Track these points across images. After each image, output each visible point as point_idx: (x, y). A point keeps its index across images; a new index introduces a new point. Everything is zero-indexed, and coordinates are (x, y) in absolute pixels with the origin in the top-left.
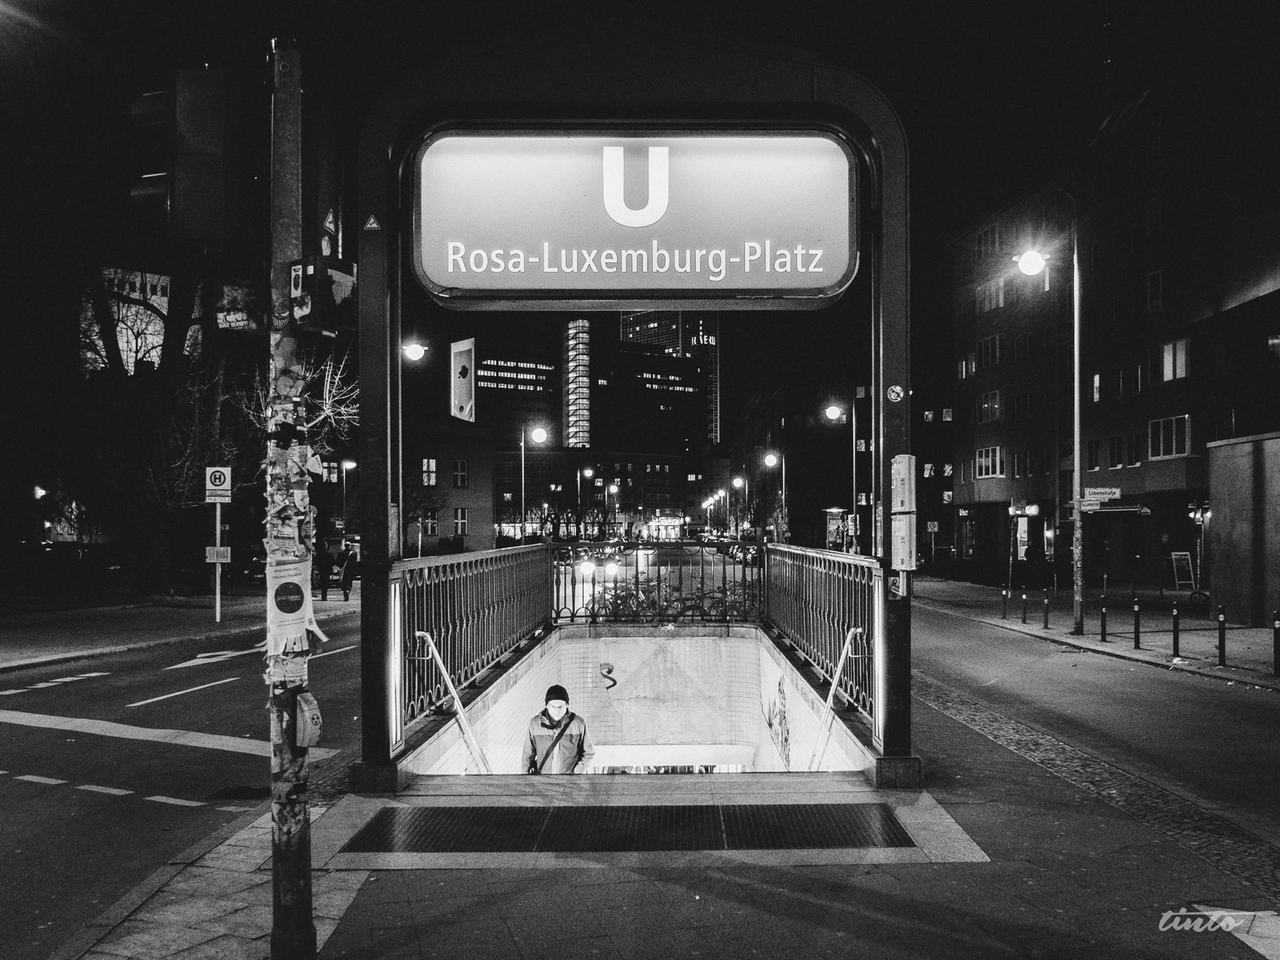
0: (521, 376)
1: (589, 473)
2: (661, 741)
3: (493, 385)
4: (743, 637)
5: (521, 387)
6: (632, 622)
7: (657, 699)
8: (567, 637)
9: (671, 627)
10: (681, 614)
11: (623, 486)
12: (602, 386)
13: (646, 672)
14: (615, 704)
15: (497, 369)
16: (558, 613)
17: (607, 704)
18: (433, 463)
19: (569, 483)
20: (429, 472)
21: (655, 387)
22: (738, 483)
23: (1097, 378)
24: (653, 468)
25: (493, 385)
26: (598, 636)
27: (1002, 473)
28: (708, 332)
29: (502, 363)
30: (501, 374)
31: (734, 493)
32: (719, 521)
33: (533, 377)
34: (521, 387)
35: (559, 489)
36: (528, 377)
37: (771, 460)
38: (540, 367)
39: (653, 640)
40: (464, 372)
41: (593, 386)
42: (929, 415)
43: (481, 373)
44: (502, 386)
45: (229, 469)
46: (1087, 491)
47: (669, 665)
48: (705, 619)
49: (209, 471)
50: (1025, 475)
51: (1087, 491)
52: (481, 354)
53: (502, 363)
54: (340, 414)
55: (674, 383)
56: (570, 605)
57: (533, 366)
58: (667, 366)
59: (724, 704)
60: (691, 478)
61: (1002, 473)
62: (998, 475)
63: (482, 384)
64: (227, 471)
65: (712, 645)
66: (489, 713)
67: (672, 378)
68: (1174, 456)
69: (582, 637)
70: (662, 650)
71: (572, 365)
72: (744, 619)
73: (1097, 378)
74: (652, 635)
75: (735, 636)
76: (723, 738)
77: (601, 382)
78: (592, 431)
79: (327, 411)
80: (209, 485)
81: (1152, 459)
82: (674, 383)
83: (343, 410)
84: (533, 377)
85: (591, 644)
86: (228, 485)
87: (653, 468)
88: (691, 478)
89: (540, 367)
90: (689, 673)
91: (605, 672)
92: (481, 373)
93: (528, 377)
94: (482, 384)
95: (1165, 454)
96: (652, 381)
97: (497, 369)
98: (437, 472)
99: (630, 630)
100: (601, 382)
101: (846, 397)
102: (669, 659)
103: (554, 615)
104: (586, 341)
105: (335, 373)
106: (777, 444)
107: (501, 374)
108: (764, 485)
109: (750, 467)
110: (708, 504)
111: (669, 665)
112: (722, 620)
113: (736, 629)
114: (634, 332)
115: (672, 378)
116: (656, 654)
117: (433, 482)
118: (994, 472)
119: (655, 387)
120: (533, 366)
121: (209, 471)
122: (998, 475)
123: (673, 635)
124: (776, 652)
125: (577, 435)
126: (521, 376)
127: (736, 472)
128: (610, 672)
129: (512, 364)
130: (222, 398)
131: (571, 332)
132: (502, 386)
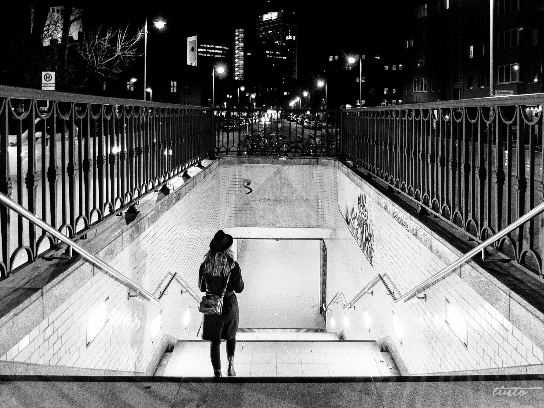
0: (216, 51)
1: (243, 89)
2: (278, 225)
3: (205, 55)
4: (326, 165)
5: (216, 56)
6: (262, 155)
7: (276, 200)
8: (223, 164)
9: (284, 158)
10: (289, 151)
11: (257, 97)
12: (249, 56)
13: (269, 185)
14: (251, 203)
15: (206, 48)
16: (218, 149)
17: (247, 203)
18: (175, 83)
19: (234, 93)
20: (174, 87)
21: (271, 56)
22: (305, 94)
23: (472, 48)
24: (270, 89)
25: (205, 55)
26: (242, 163)
27: (425, 90)
28: (292, 35)
29: (208, 46)
30: (208, 50)
31: (303, 99)
32: (297, 111)
33: (221, 52)
34: (216, 56)
35: (231, 97)
36: (219, 52)
37: (321, 84)
38: (224, 48)
39: (274, 166)
40: (193, 49)
41: (245, 56)
42: (386, 68)
43: (199, 50)
44: (208, 55)
45: (54, 73)
46: (496, 91)
47: (283, 181)
48: (304, 154)
49: (44, 73)
50: (436, 90)
51: (496, 91)
52: (200, 43)
53: (208, 46)
54: (125, 54)
55: (278, 55)
56: (225, 145)
57: (221, 47)
58: (275, 48)
59: (315, 204)
60: (285, 93)
61: (425, 90)
62: (424, 91)
63: (200, 54)
64: (53, 74)
65: (308, 170)
66: (144, 234)
67: (277, 53)
68: (511, 82)
69: (232, 163)
70: (279, 172)
71: (237, 47)
72: (327, 154)
73: (472, 48)
74: (273, 163)
75: (321, 165)
76: (314, 224)
77: (248, 54)
78: (244, 74)
79: (119, 52)
80: (43, 81)
81: (499, 83)
82: (278, 55)
83: (126, 52)
84: (221, 52)
85: (237, 169)
86: (53, 81)
87: (270, 89)
88: (285, 93)
89: (224, 48)
90: (294, 185)
91: (246, 184)
92: (199, 50)
93: (219, 52)
94: (200, 54)
95: (512, 81)
96: (269, 54)
97: (206, 48)
98: (177, 87)
99: (260, 159)
100: (248, 54)
101: (247, 154)
102: (283, 177)
103: (216, 150)
104: (243, 46)
105: (122, 35)
106: (323, 77)
107: (208, 50)
108: (317, 94)
109: (311, 87)
110: (292, 104)
111: (283, 181)
112: (316, 155)
113: (323, 160)
114: (262, 34)
115: (277, 53)
116: (275, 174)
117: (175, 90)
118: (422, 89)
119: (271, 56)
120: (221, 47)
121: (44, 73)
122: (424, 91)
123: (286, 163)
124: (357, 178)
125: (238, 75)
126: (216, 51)
127: (304, 89)
128: (248, 184)
129: (212, 46)
130: (68, 46)
131: (237, 33)
132: (208, 55)
